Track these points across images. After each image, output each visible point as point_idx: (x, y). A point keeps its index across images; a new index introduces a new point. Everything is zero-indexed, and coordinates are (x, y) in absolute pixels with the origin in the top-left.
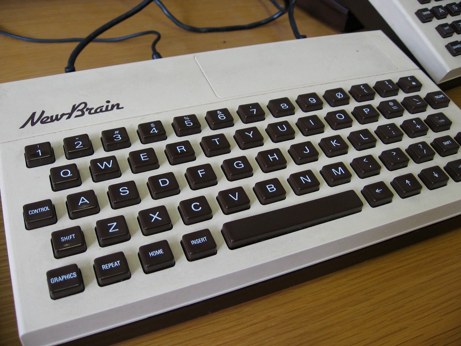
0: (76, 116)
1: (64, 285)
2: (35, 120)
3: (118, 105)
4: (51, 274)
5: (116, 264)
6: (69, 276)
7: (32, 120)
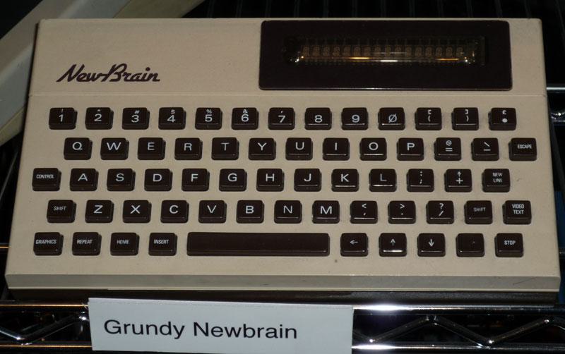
0: (112, 80)
1: (510, 247)
2: (72, 75)
3: (156, 75)
4: (39, 236)
5: (88, 242)
6: (50, 242)
7: (70, 75)
